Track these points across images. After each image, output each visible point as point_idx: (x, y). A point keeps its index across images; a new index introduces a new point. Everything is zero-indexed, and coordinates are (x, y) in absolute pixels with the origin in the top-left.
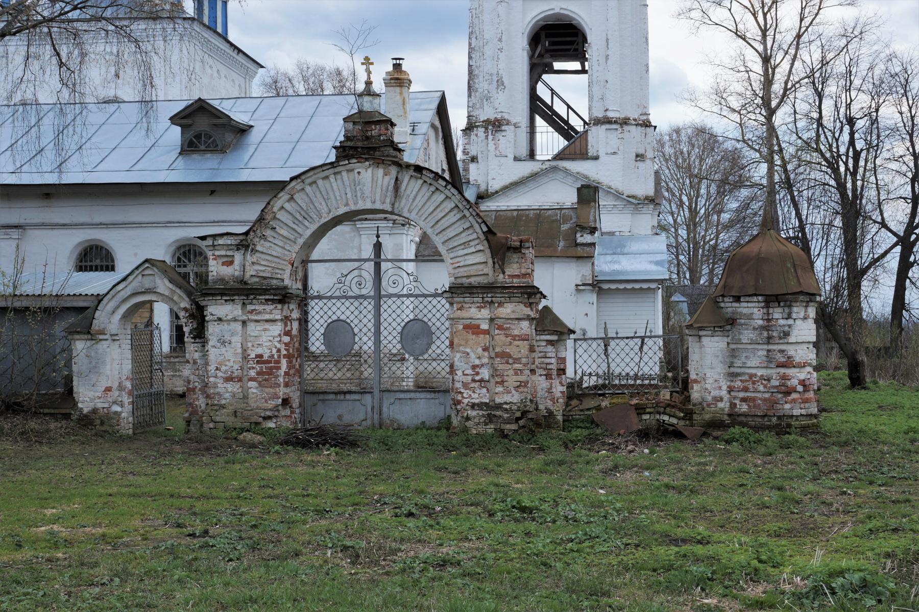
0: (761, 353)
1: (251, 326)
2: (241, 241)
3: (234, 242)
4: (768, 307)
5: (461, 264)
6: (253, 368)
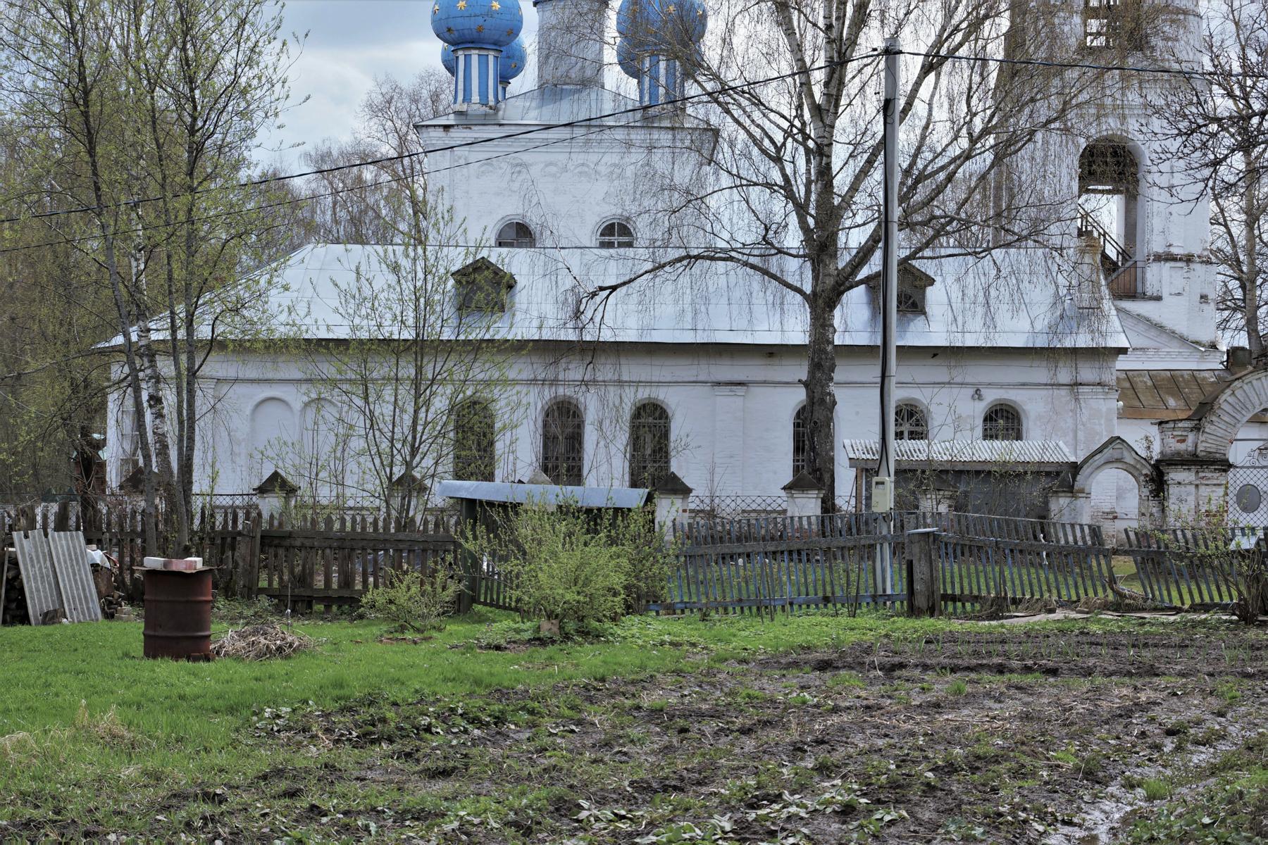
1: (1202, 489)
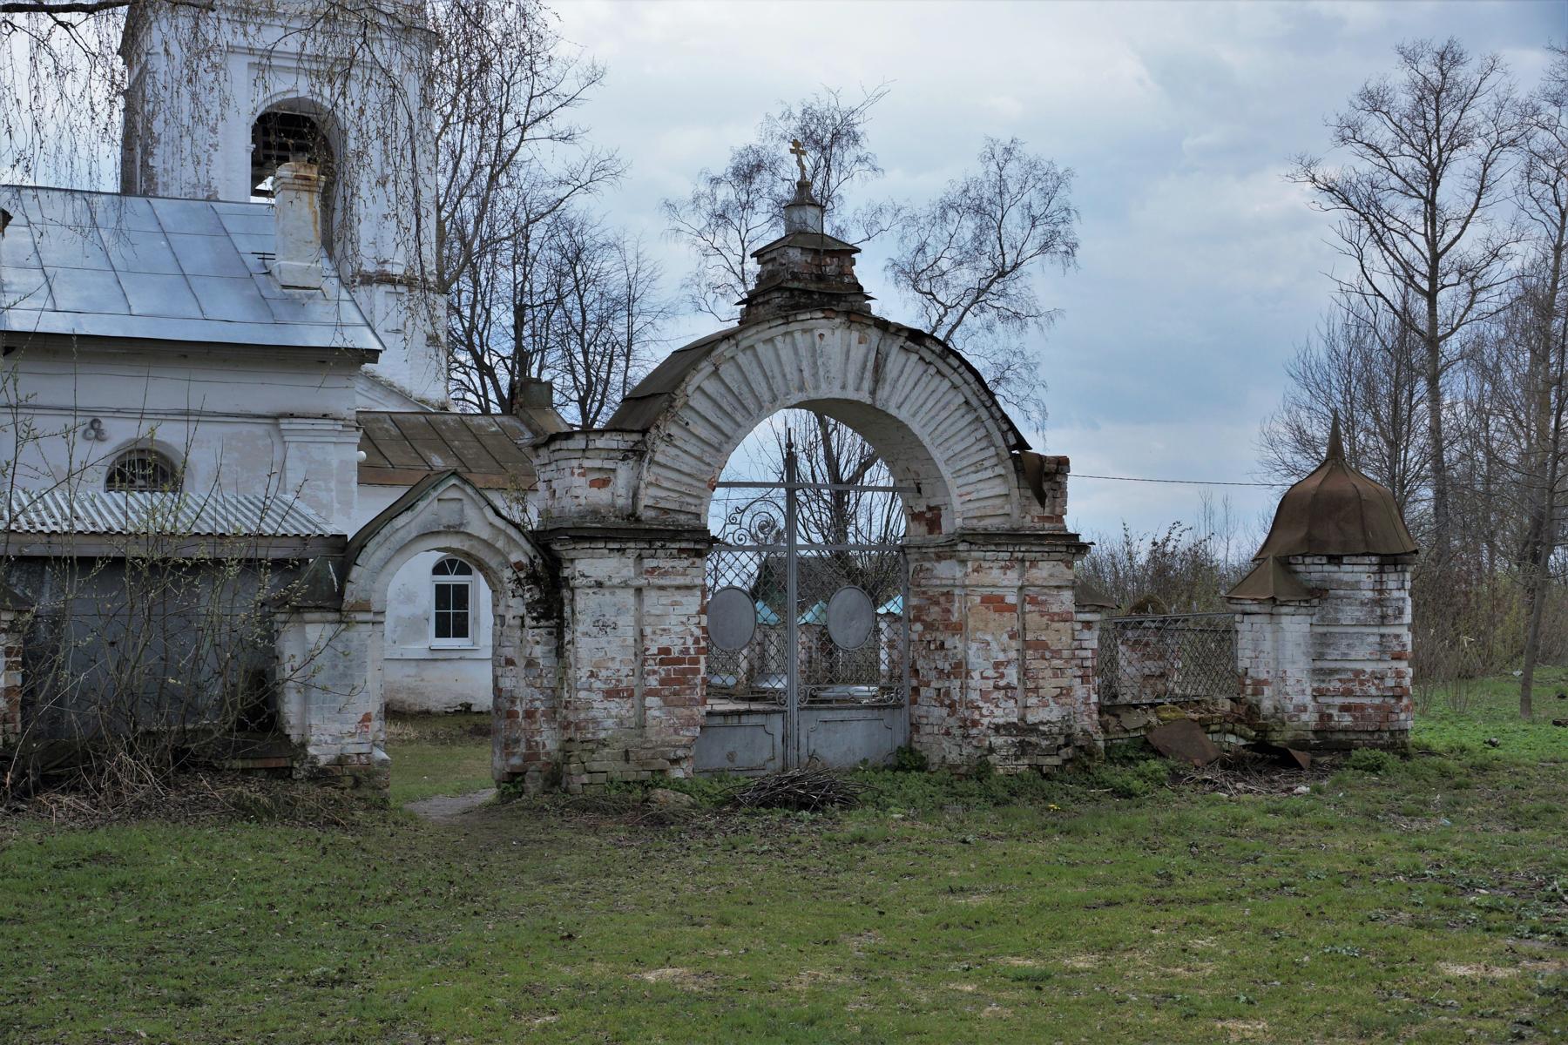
0: (1372, 639)
1: (651, 597)
2: (636, 443)
3: (622, 446)
4: (1381, 572)
5: (973, 497)
6: (655, 672)
